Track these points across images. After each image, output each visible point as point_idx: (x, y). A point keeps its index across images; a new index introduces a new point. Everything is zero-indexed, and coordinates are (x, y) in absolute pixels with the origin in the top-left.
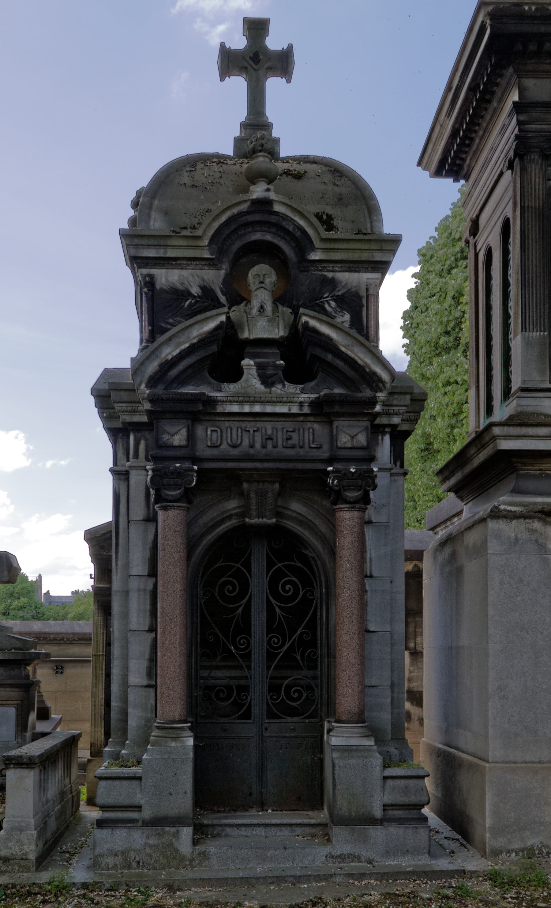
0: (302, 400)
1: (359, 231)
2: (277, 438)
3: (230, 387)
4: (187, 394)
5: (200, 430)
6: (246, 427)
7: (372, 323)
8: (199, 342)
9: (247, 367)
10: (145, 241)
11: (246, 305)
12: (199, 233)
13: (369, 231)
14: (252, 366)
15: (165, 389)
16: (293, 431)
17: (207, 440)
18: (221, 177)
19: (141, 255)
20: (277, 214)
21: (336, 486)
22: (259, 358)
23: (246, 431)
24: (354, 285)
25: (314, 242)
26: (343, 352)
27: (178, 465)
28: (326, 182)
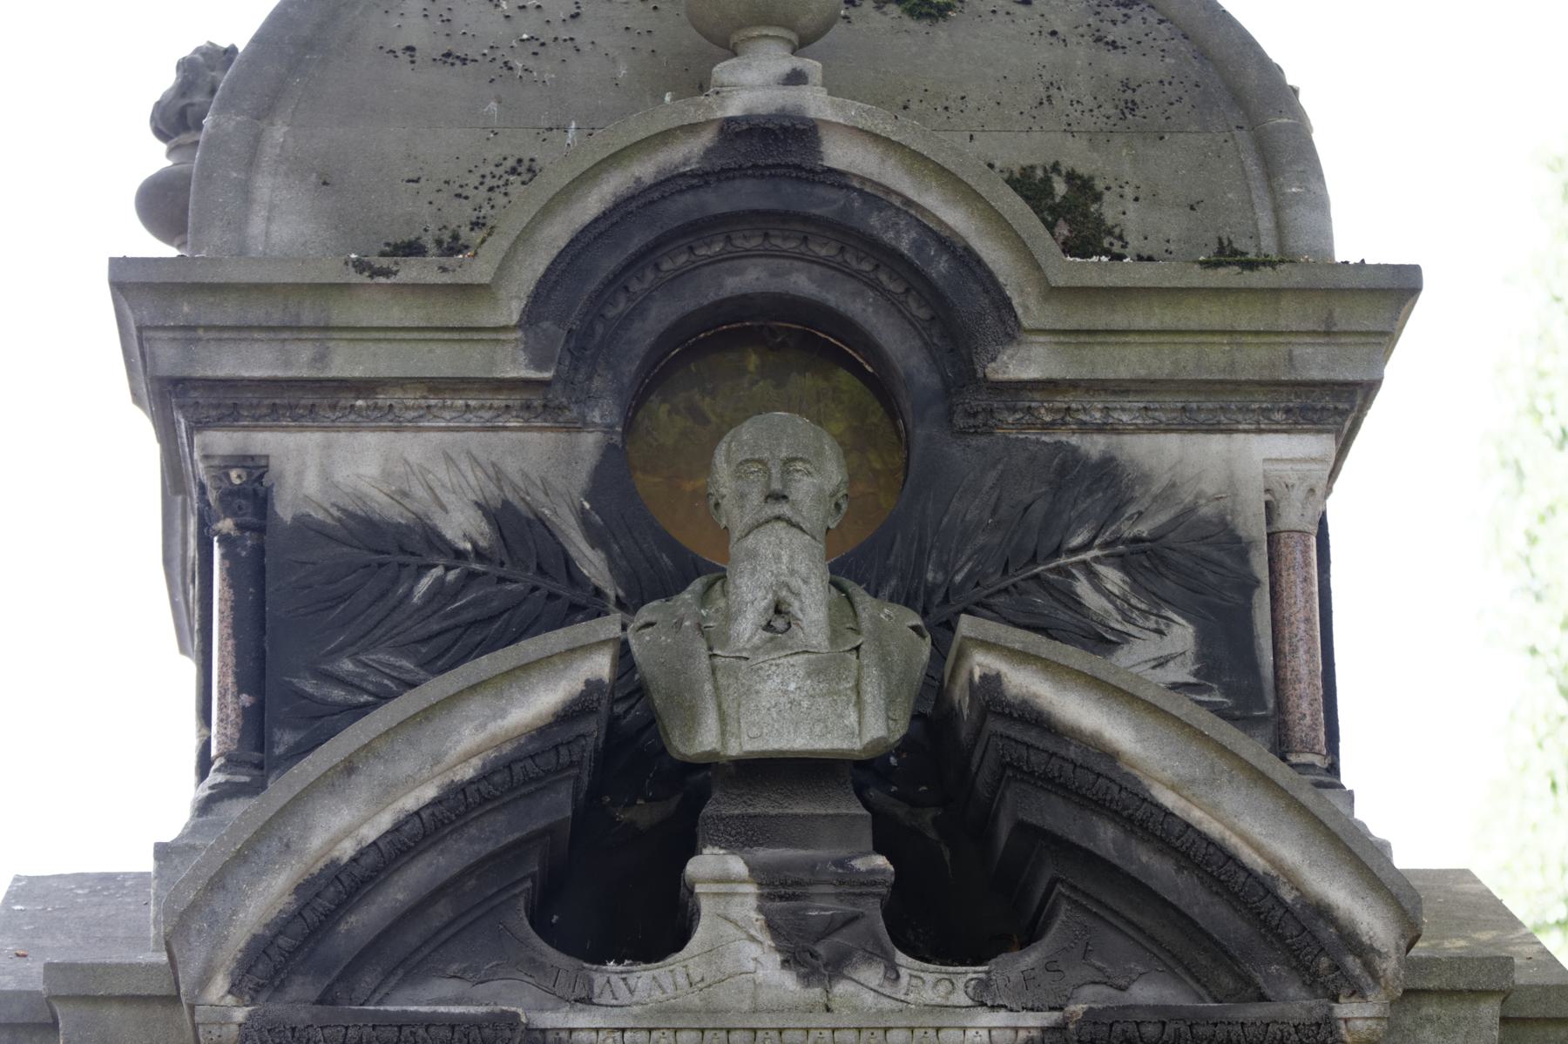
1: (1221, 251)
3: (632, 981)
7: (1304, 664)
8: (484, 776)
9: (715, 888)
10: (229, 312)
11: (704, 598)
12: (479, 270)
13: (1268, 245)
14: (743, 882)
18: (575, 16)
19: (209, 373)
20: (838, 179)
22: (771, 842)
24: (1210, 489)
26: (1168, 813)
28: (1061, 29)
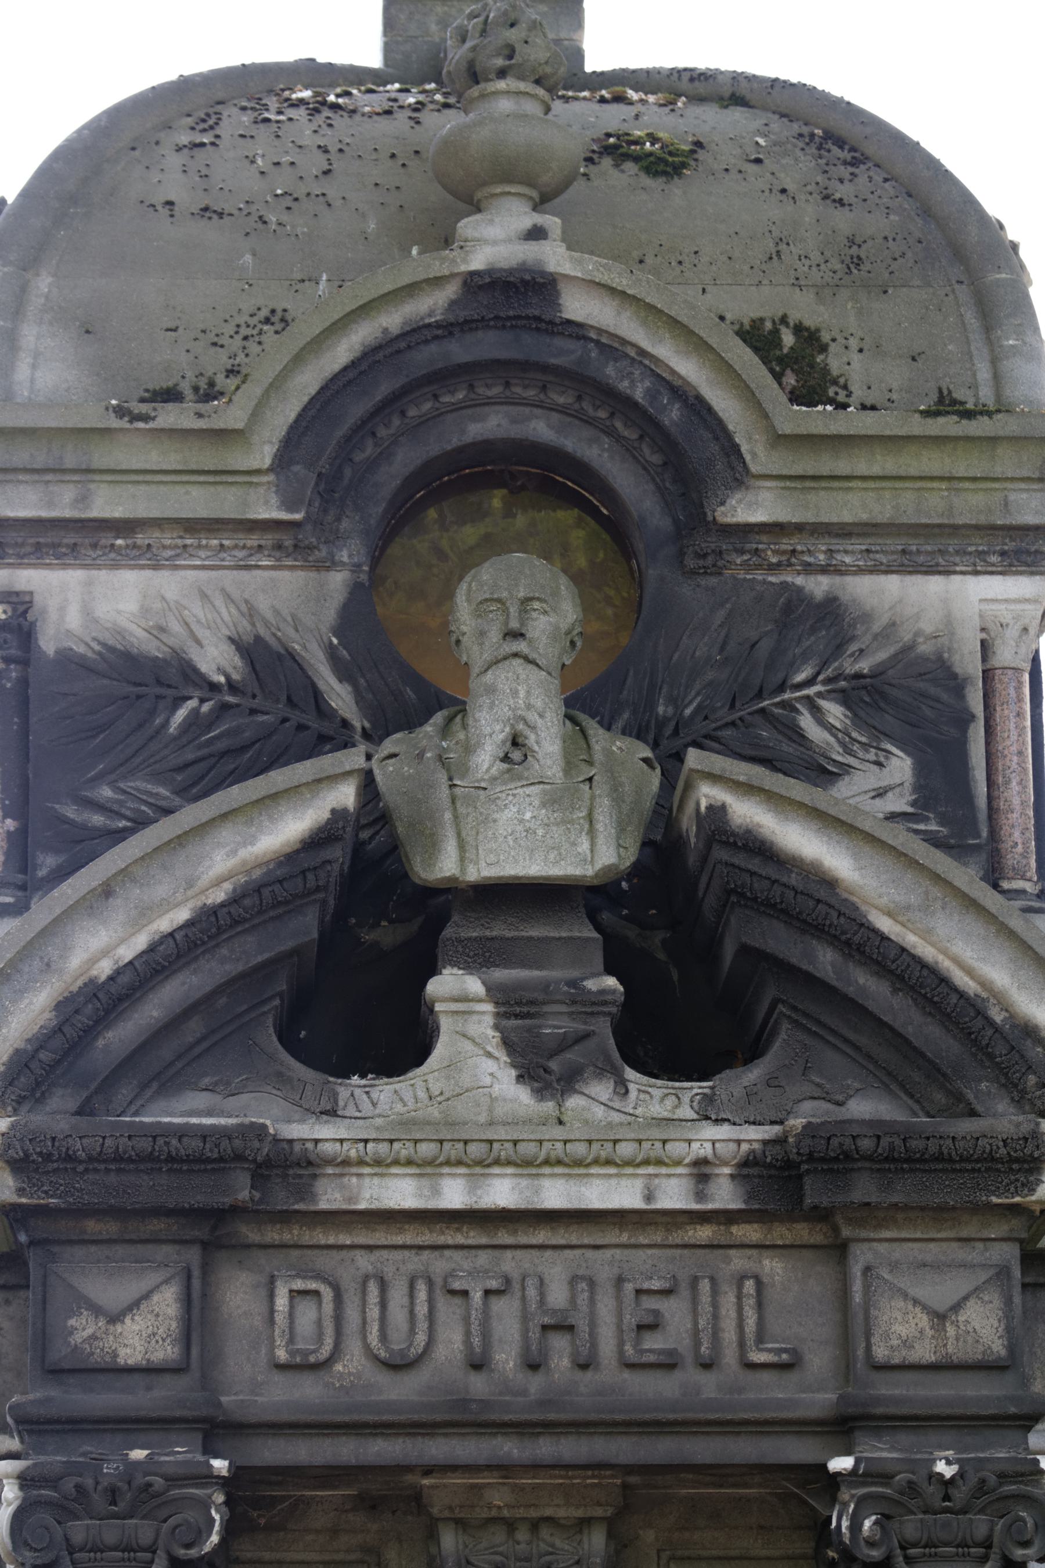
0: (707, 1150)
2: (593, 1325)
3: (375, 1095)
4: (182, 1133)
5: (238, 1294)
6: (451, 1274)
12: (232, 415)
13: (986, 395)
14: (480, 1001)
15: (83, 1111)
16: (667, 1293)
17: (272, 1340)
18: (327, 172)
20: (576, 330)
21: (871, 1544)
23: (453, 1292)
24: (928, 628)
25: (744, 449)
26: (884, 938)
27: (138, 1454)
28: (791, 187)
